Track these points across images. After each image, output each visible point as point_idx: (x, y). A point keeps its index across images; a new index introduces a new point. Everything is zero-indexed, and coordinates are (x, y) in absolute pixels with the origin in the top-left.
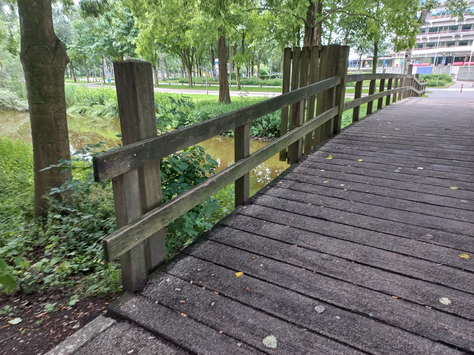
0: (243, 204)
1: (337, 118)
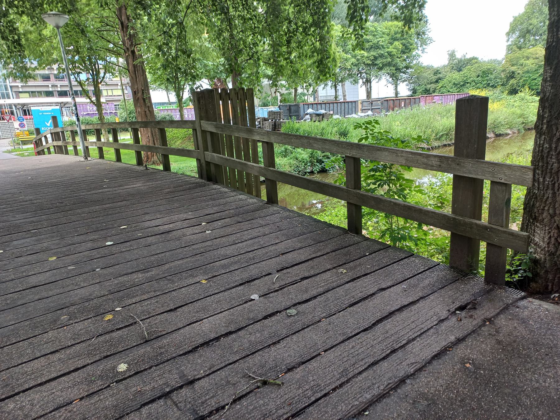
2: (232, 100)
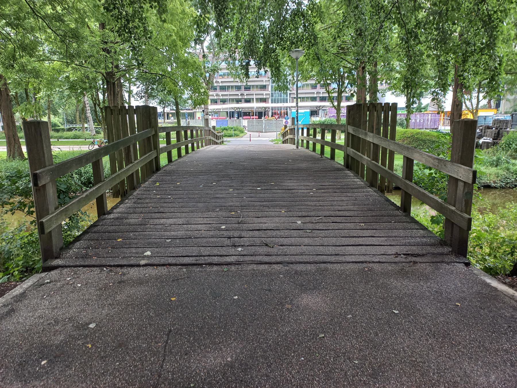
0: (104, 214)
1: (157, 159)
2: (377, 111)
